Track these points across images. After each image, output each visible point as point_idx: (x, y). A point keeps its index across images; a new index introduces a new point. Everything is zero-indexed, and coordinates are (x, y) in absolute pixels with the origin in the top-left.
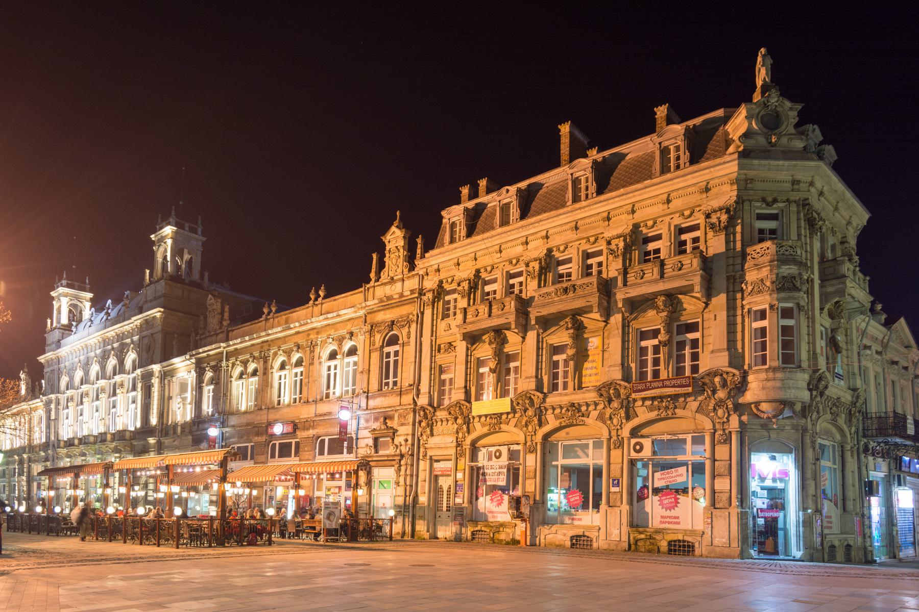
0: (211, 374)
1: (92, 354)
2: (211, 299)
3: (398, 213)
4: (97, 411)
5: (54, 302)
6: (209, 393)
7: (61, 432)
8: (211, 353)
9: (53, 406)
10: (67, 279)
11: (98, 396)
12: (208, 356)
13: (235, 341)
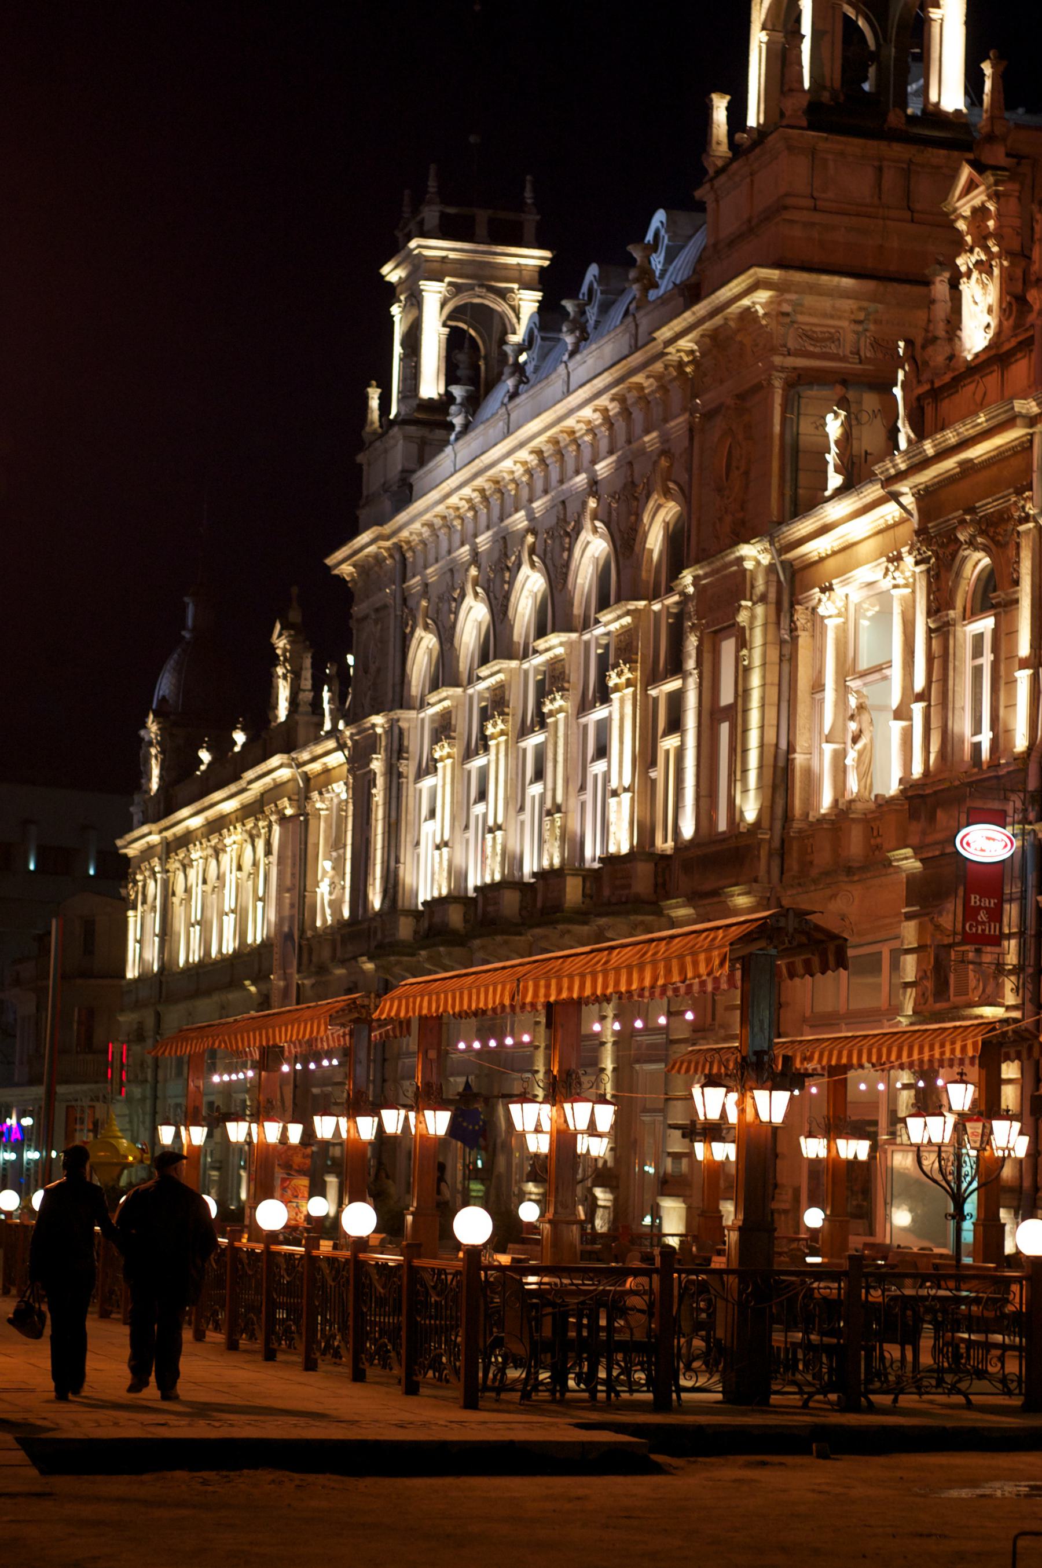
0: (986, 561)
1: (519, 520)
2: (971, 186)
3: (295, 590)
4: (539, 775)
5: (395, 310)
6: (978, 652)
7: (407, 876)
8: (977, 452)
9: (377, 765)
10: (445, 199)
11: (602, 678)
12: (968, 468)
13: (966, 430)
